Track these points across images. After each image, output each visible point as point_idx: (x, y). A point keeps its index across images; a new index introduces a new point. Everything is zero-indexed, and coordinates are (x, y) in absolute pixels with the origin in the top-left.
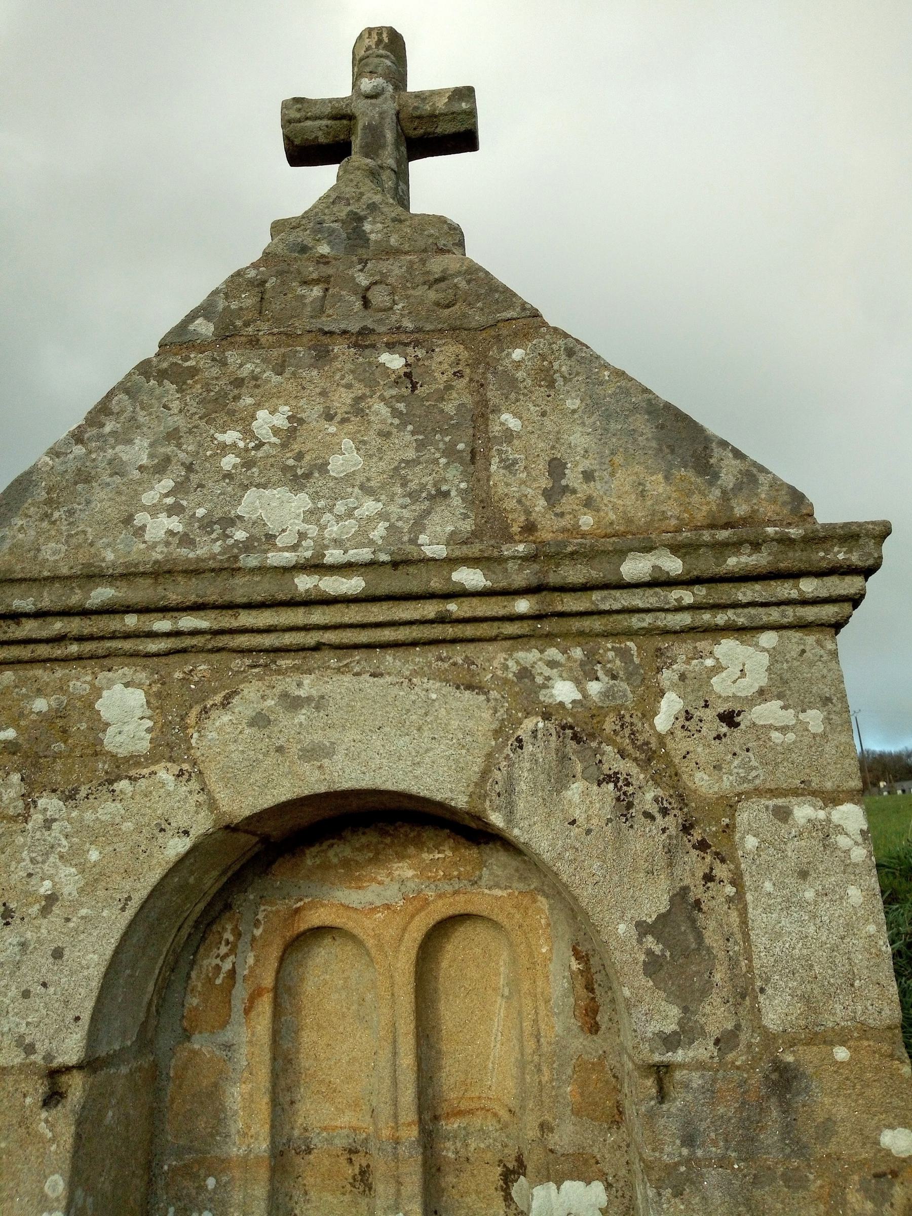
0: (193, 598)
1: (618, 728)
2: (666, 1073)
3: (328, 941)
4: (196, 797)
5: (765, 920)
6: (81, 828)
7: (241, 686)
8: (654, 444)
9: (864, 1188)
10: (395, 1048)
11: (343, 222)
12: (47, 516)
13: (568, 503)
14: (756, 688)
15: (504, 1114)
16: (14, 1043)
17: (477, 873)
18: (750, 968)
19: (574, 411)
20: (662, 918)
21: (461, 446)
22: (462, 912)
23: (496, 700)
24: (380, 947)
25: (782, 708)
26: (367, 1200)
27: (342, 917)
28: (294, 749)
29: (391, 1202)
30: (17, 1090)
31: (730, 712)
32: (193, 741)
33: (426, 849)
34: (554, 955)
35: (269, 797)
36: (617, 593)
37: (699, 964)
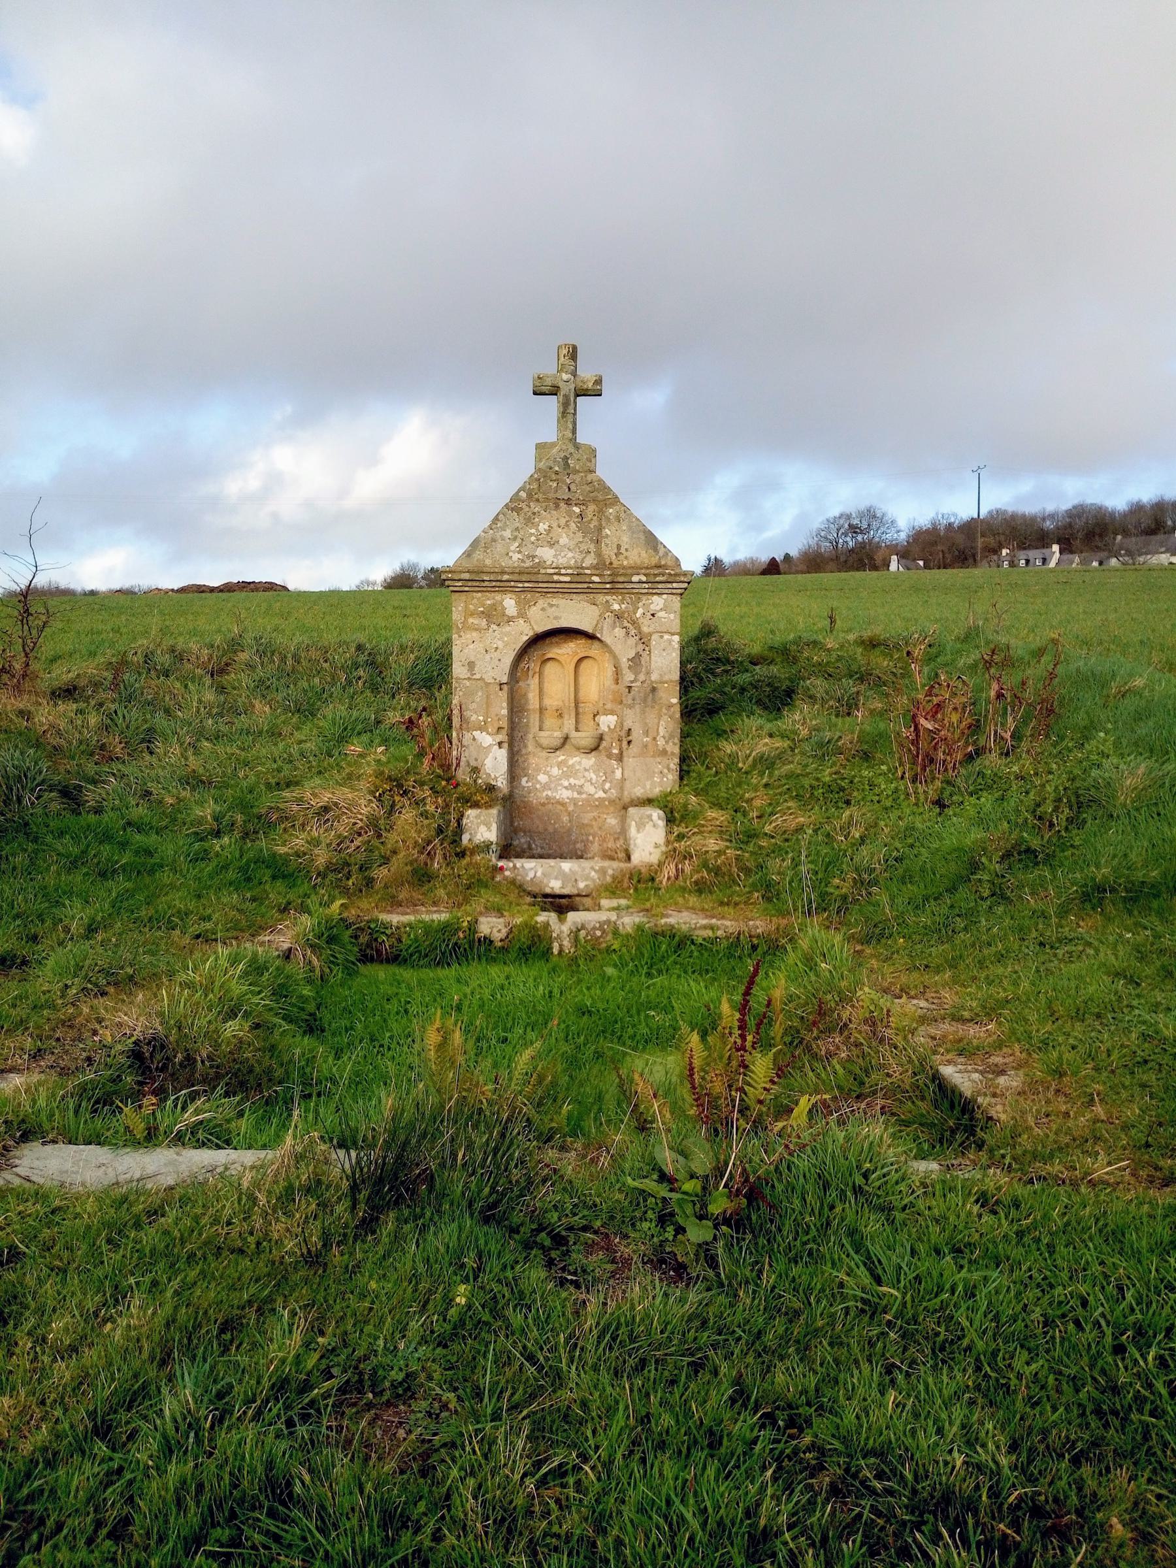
6: (501, 632)
13: (621, 557)
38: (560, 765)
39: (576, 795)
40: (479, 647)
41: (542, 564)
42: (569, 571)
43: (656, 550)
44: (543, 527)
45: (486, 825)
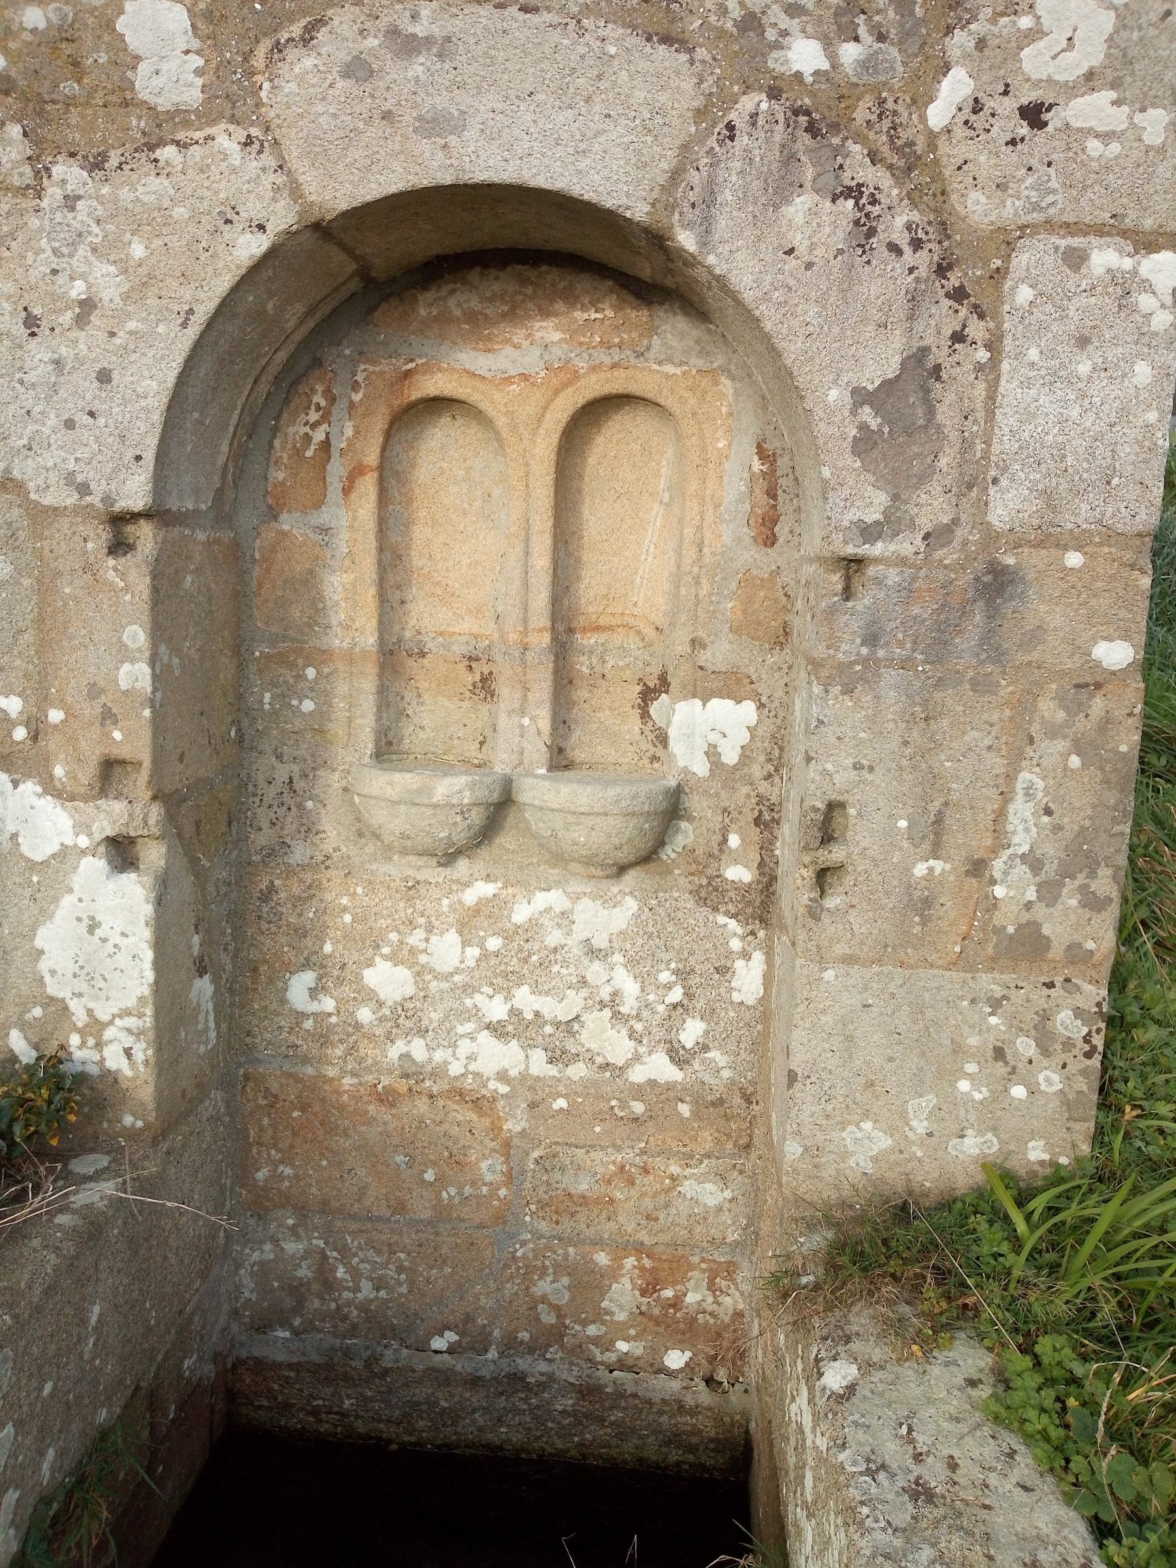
1: (874, 117)
2: (856, 571)
3: (445, 420)
4: (272, 177)
5: (1019, 396)
7: (330, 13)
9: (1060, 699)
10: (527, 546)
14: (1084, 69)
16: (62, 482)
17: (645, 342)
18: (986, 456)
20: (888, 385)
22: (621, 391)
23: (703, 62)
24: (514, 428)
25: (1113, 103)
26: (488, 706)
27: (466, 387)
28: (408, 117)
29: (517, 705)
30: (74, 533)
31: (1036, 105)
32: (263, 94)
33: (579, 306)
34: (733, 452)
35: (373, 185)
37: (923, 445)
39: (538, 1064)
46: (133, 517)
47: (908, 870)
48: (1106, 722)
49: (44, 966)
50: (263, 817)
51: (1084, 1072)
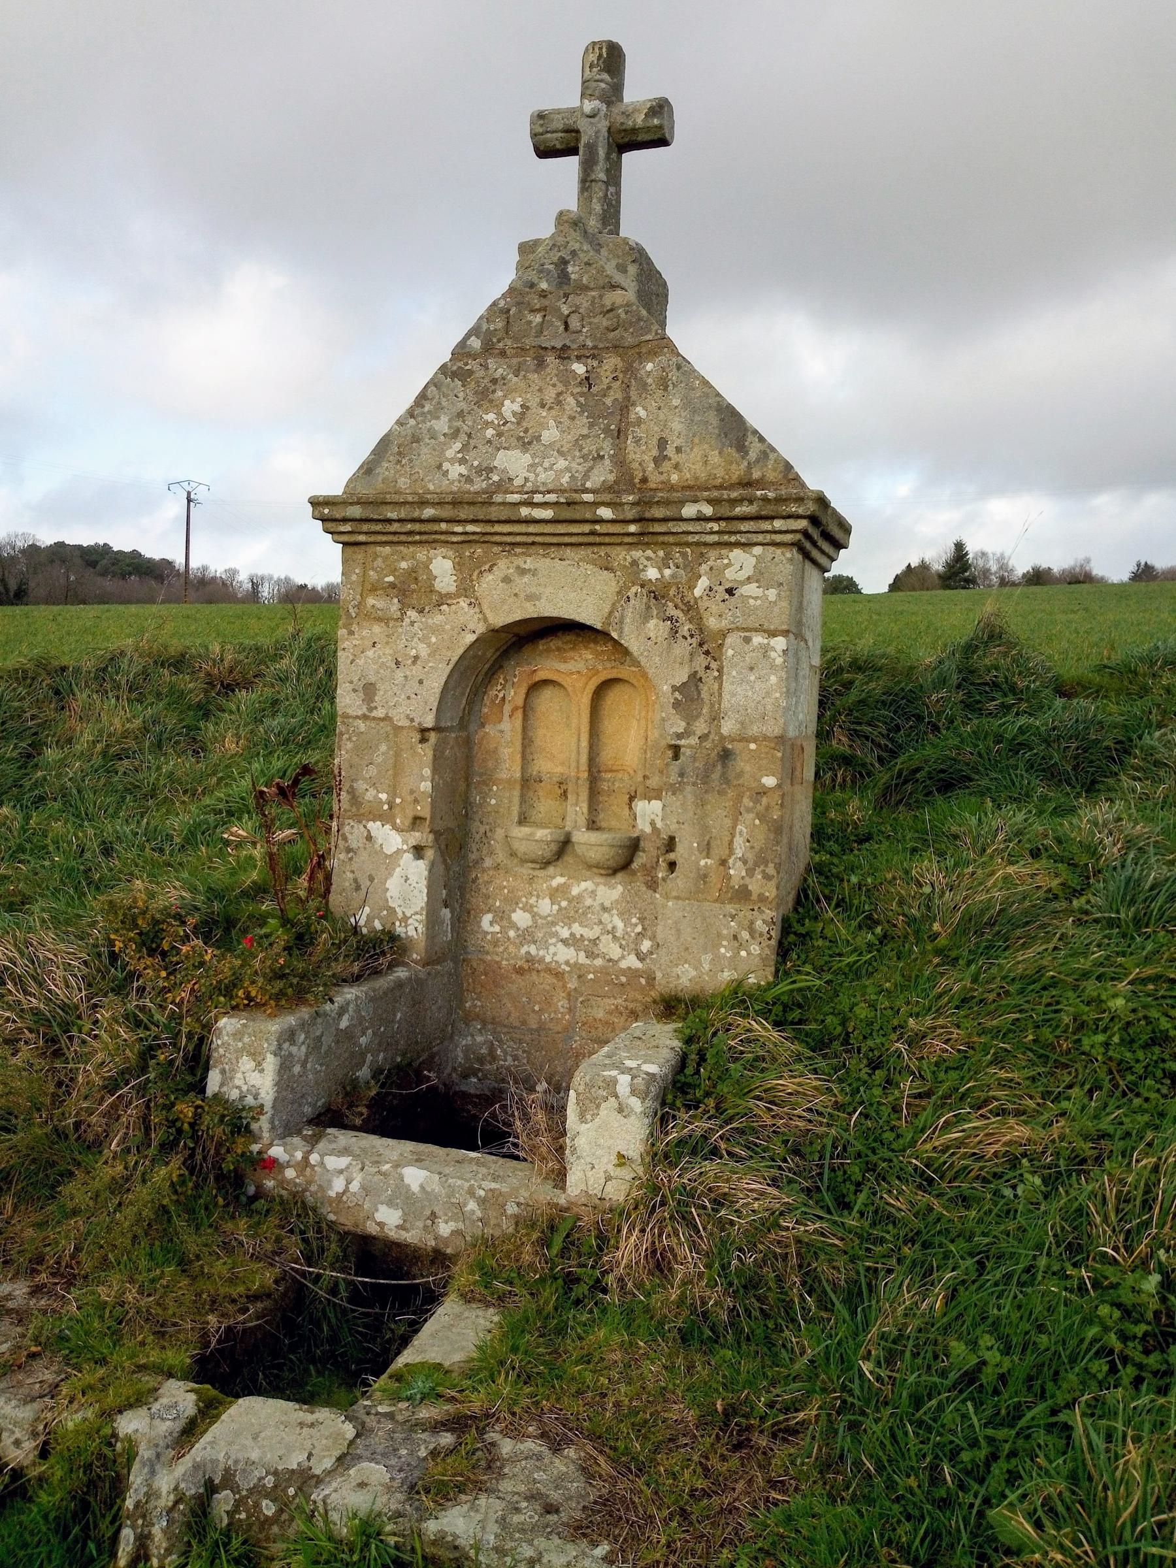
0: (472, 517)
3: (551, 687)
6: (427, 627)
8: (717, 431)
9: (751, 798)
11: (556, 265)
12: (399, 462)
13: (666, 466)
15: (632, 772)
18: (719, 708)
19: (676, 407)
21: (613, 427)
28: (522, 595)
36: (681, 523)
38: (555, 894)
39: (582, 958)
40: (385, 654)
41: (504, 485)
42: (552, 498)
43: (742, 448)
44: (510, 407)
45: (253, 1055)
46: (428, 730)
47: (698, 863)
48: (768, 808)
49: (388, 894)
50: (474, 847)
51: (768, 946)
